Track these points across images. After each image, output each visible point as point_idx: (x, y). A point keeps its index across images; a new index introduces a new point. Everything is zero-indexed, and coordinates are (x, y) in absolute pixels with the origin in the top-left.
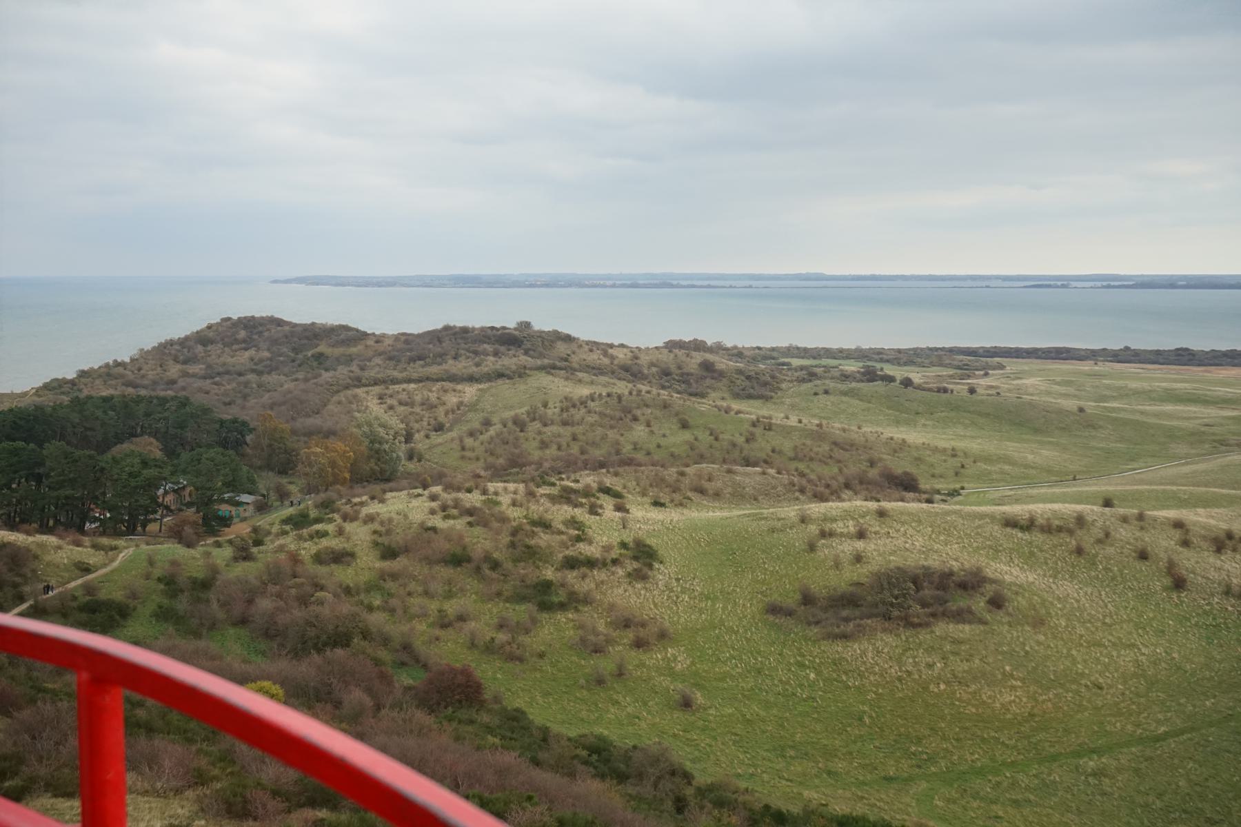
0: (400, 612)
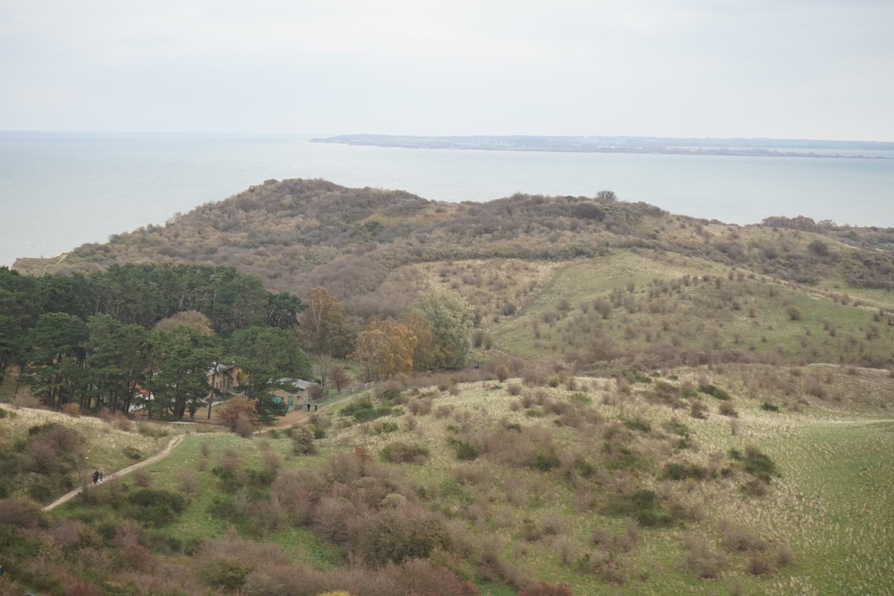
0: (481, 520)
